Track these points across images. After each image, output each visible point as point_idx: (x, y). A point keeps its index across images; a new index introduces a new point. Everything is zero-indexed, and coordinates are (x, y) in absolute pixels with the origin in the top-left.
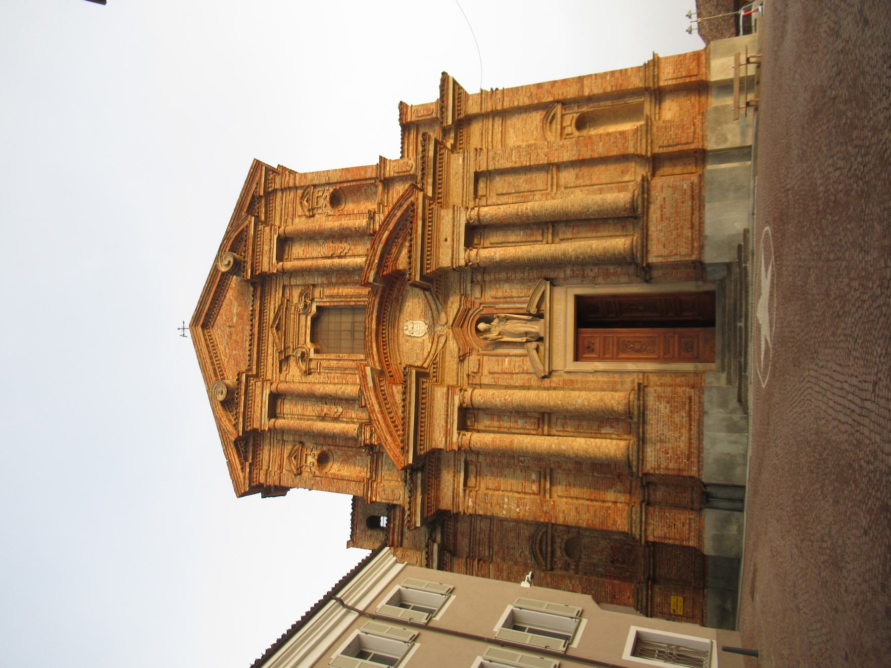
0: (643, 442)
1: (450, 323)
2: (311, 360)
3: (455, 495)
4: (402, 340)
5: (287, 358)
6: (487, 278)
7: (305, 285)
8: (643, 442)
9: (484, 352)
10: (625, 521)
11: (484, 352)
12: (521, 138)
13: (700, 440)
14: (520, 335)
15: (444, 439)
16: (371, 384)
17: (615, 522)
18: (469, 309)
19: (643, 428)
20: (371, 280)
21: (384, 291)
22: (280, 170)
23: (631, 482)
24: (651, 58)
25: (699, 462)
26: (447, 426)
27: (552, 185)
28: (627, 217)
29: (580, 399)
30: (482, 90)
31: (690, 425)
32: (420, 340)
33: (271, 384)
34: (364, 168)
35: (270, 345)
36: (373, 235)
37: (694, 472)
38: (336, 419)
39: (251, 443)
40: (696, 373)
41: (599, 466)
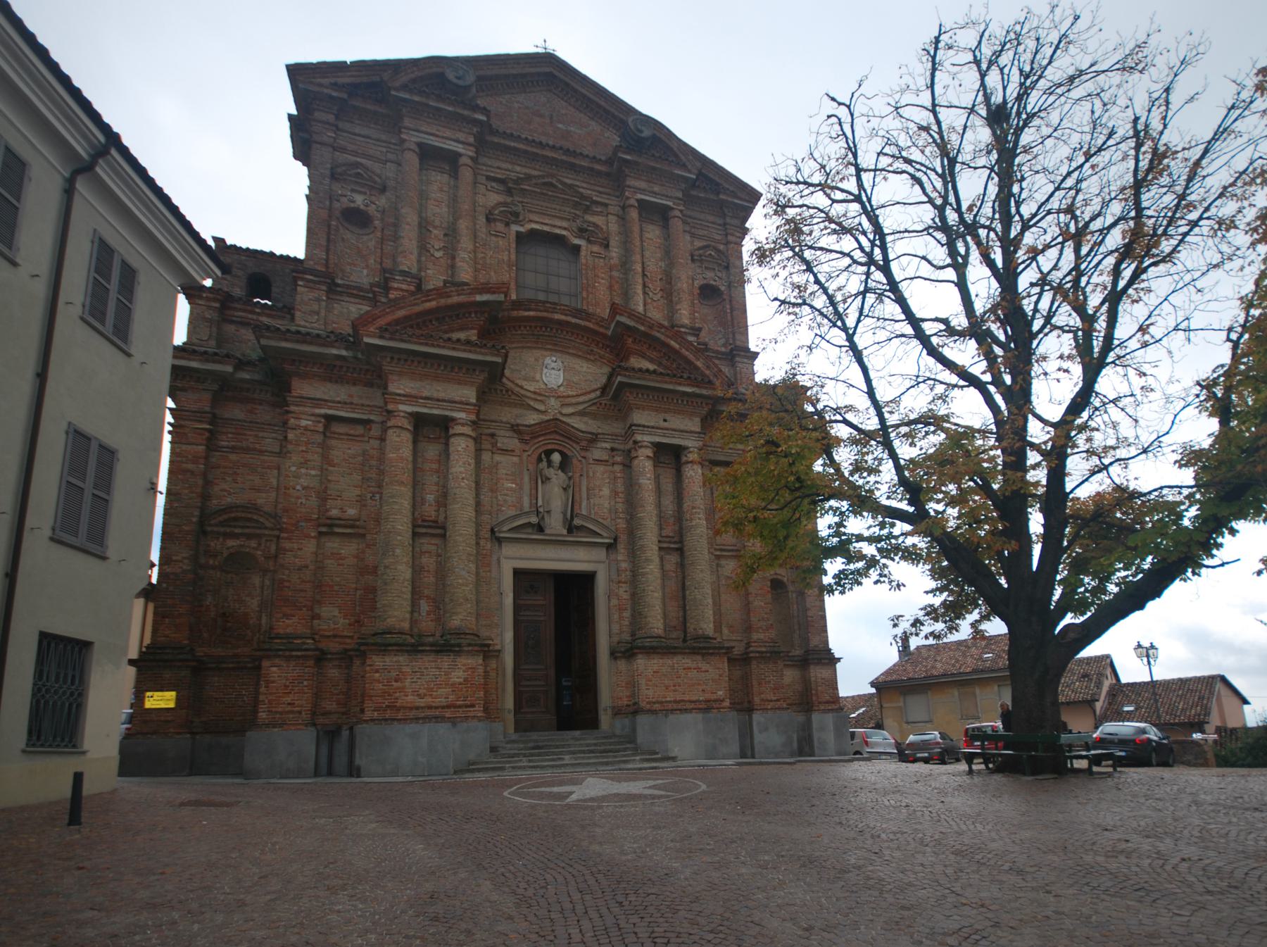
2: (507, 224)
4: (537, 353)
5: (509, 192)
16: (479, 298)
17: (287, 616)
20: (618, 318)
23: (351, 637)
24: (837, 656)
25: (386, 720)
28: (685, 632)
31: (436, 708)
32: (538, 377)
37: (368, 714)
41: (371, 596)
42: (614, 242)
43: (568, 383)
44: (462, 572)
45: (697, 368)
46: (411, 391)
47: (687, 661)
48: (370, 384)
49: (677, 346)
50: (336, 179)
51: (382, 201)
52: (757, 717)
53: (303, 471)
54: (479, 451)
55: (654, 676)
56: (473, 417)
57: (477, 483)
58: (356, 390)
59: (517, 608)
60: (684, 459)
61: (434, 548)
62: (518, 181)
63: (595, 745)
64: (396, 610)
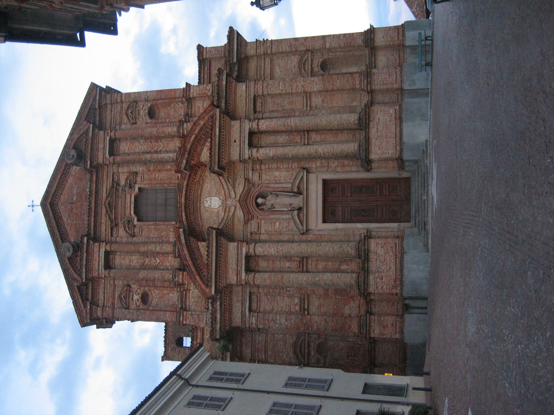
0: (367, 273)
1: (238, 198)
2: (135, 226)
3: (243, 315)
4: (203, 211)
6: (263, 167)
8: (367, 273)
13: (402, 270)
14: (285, 205)
16: (183, 241)
17: (350, 327)
18: (251, 189)
19: (368, 264)
23: (360, 300)
24: (369, 27)
25: (401, 283)
26: (238, 268)
27: (307, 106)
28: (356, 129)
30: (257, 40)
31: (396, 261)
32: (216, 210)
38: (156, 268)
39: (90, 287)
41: (339, 291)
42: (133, 169)
43: (217, 194)
44: (327, 249)
45: (204, 124)
46: (234, 273)
47: (373, 132)
48: (231, 292)
49: (193, 136)
51: (134, 287)
52: (406, 87)
53: (278, 321)
54: (260, 241)
55: (382, 148)
56: (245, 244)
57: (278, 242)
58: (235, 299)
59: (343, 221)
60: (256, 130)
62: (111, 222)
63: (418, 182)
64: (347, 279)
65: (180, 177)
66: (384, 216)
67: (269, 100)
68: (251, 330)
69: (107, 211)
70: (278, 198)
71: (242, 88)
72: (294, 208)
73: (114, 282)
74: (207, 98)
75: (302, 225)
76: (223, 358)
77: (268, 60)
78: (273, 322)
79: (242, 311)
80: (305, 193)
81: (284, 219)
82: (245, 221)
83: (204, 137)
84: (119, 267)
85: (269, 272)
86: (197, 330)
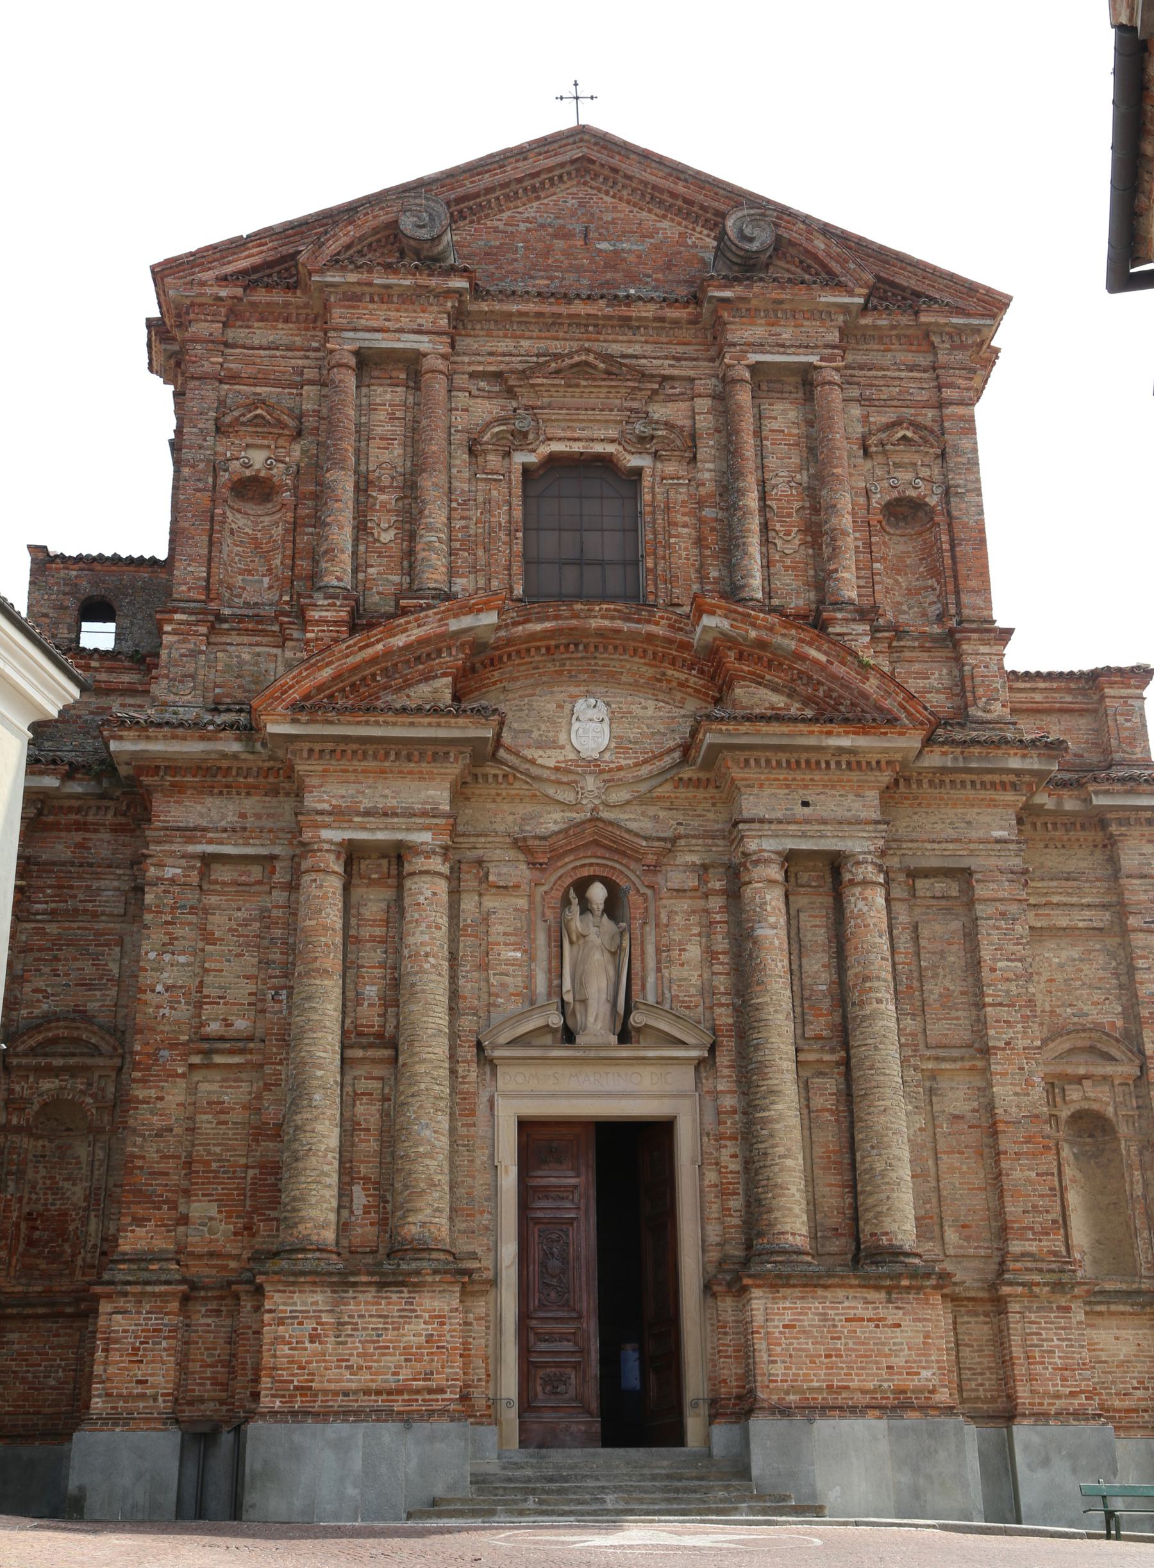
1: (605, 814)
2: (507, 455)
3: (190, 833)
4: (561, 693)
7: (693, 436)
9: (538, 899)
10: (142, 1245)
11: (538, 899)
12: (1059, 977)
13: (345, 1414)
14: (579, 982)
15: (326, 806)
17: (140, 1221)
18: (638, 860)
21: (685, 646)
22: (984, 353)
23: (237, 1257)
25: (294, 1414)
26: (358, 814)
29: (430, 1133)
31: (378, 1393)
32: (562, 739)
33: (444, 357)
34: (984, 589)
35: (542, 345)
36: (815, 622)
38: (361, 528)
40: (493, 1402)
41: (271, 1180)
42: (707, 449)
43: (620, 744)
48: (275, 792)
49: (823, 658)
50: (226, 434)
53: (167, 957)
54: (455, 893)
56: (445, 839)
58: (251, 804)
61: (375, 1085)
62: (523, 374)
65: (679, 611)
66: (543, 1346)
67: (956, 925)
68: (138, 861)
69: (557, 357)
70: (607, 956)
71: (999, 825)
72: (574, 1012)
73: (311, 382)
74: (958, 701)
75: (511, 1043)
76: (38, 761)
77: (1102, 918)
78: (166, 939)
79: (205, 830)
80: (625, 1054)
81: (530, 977)
82: (525, 839)
83: (821, 694)
84: (364, 401)
85: (346, 926)
86: (139, 671)
